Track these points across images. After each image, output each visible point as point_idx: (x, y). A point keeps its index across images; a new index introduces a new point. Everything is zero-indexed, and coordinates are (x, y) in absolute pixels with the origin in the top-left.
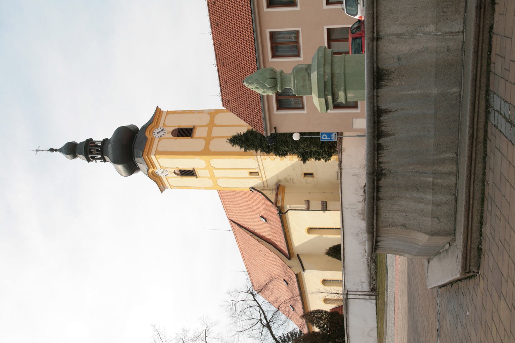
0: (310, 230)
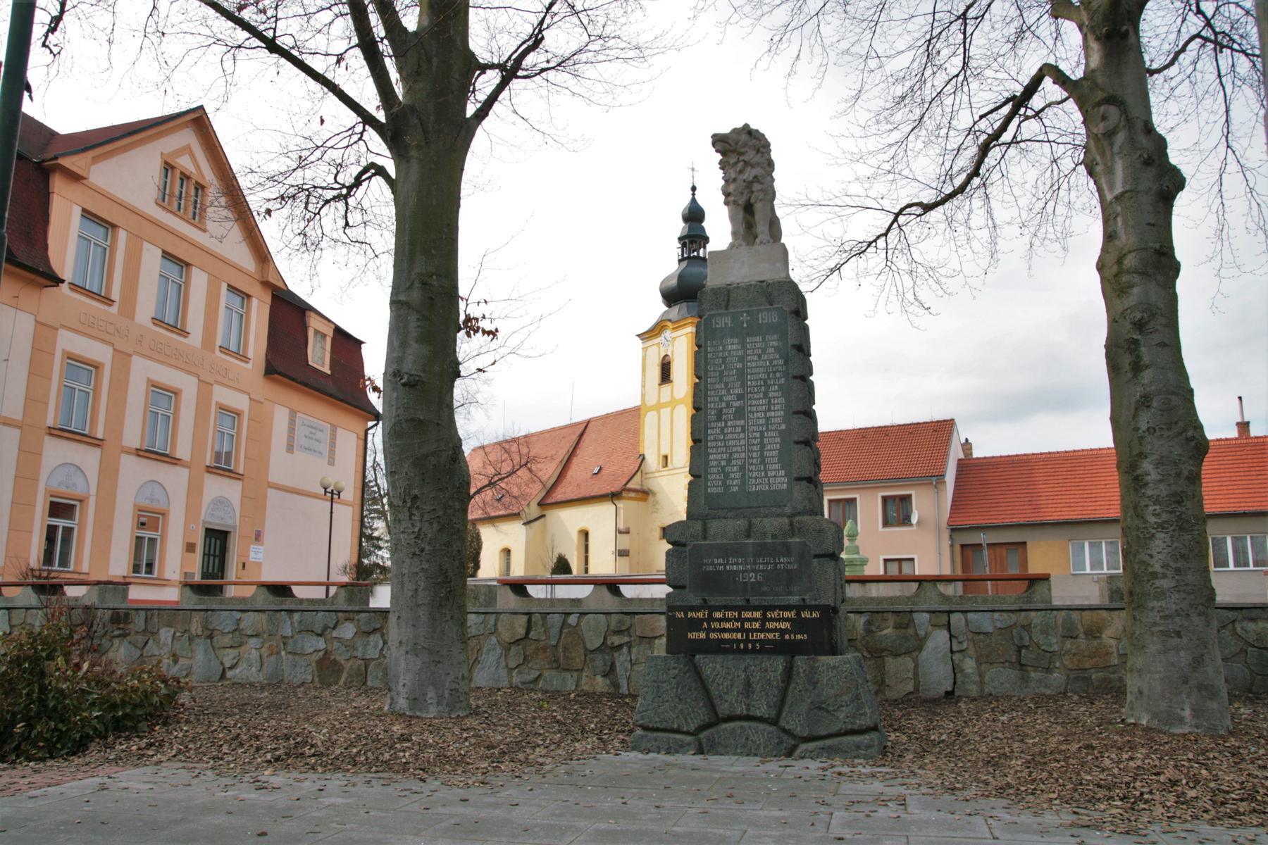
0: (585, 534)
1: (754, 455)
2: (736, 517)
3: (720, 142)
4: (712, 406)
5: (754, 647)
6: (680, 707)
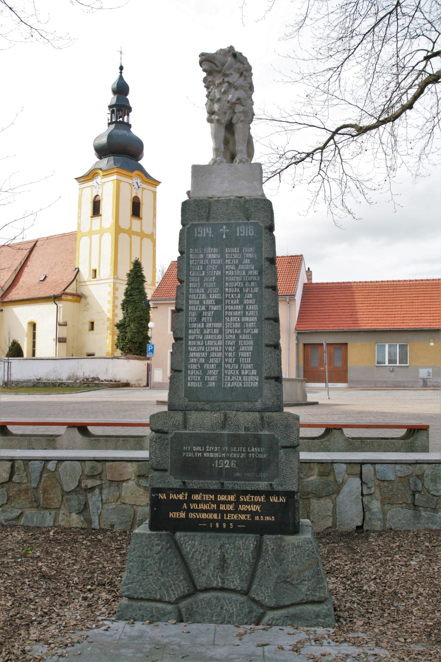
0: (34, 326)
1: (230, 355)
2: (212, 410)
3: (206, 60)
4: (193, 308)
5: (228, 525)
6: (162, 579)
